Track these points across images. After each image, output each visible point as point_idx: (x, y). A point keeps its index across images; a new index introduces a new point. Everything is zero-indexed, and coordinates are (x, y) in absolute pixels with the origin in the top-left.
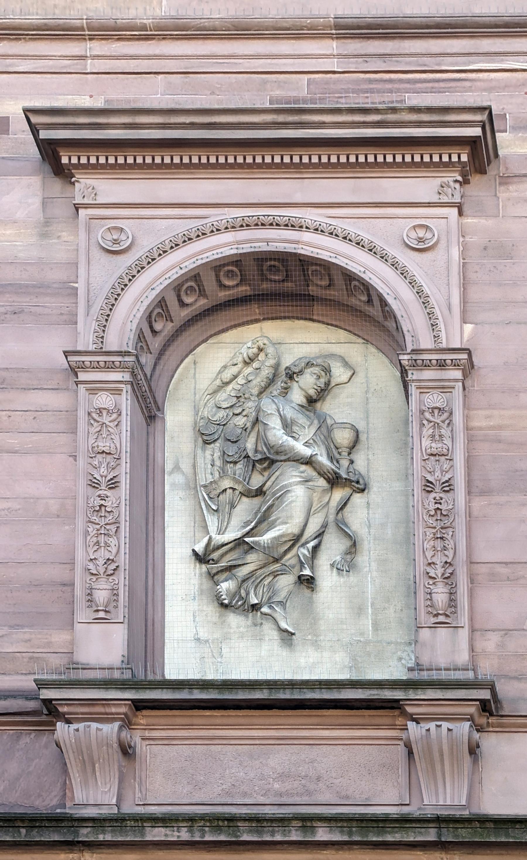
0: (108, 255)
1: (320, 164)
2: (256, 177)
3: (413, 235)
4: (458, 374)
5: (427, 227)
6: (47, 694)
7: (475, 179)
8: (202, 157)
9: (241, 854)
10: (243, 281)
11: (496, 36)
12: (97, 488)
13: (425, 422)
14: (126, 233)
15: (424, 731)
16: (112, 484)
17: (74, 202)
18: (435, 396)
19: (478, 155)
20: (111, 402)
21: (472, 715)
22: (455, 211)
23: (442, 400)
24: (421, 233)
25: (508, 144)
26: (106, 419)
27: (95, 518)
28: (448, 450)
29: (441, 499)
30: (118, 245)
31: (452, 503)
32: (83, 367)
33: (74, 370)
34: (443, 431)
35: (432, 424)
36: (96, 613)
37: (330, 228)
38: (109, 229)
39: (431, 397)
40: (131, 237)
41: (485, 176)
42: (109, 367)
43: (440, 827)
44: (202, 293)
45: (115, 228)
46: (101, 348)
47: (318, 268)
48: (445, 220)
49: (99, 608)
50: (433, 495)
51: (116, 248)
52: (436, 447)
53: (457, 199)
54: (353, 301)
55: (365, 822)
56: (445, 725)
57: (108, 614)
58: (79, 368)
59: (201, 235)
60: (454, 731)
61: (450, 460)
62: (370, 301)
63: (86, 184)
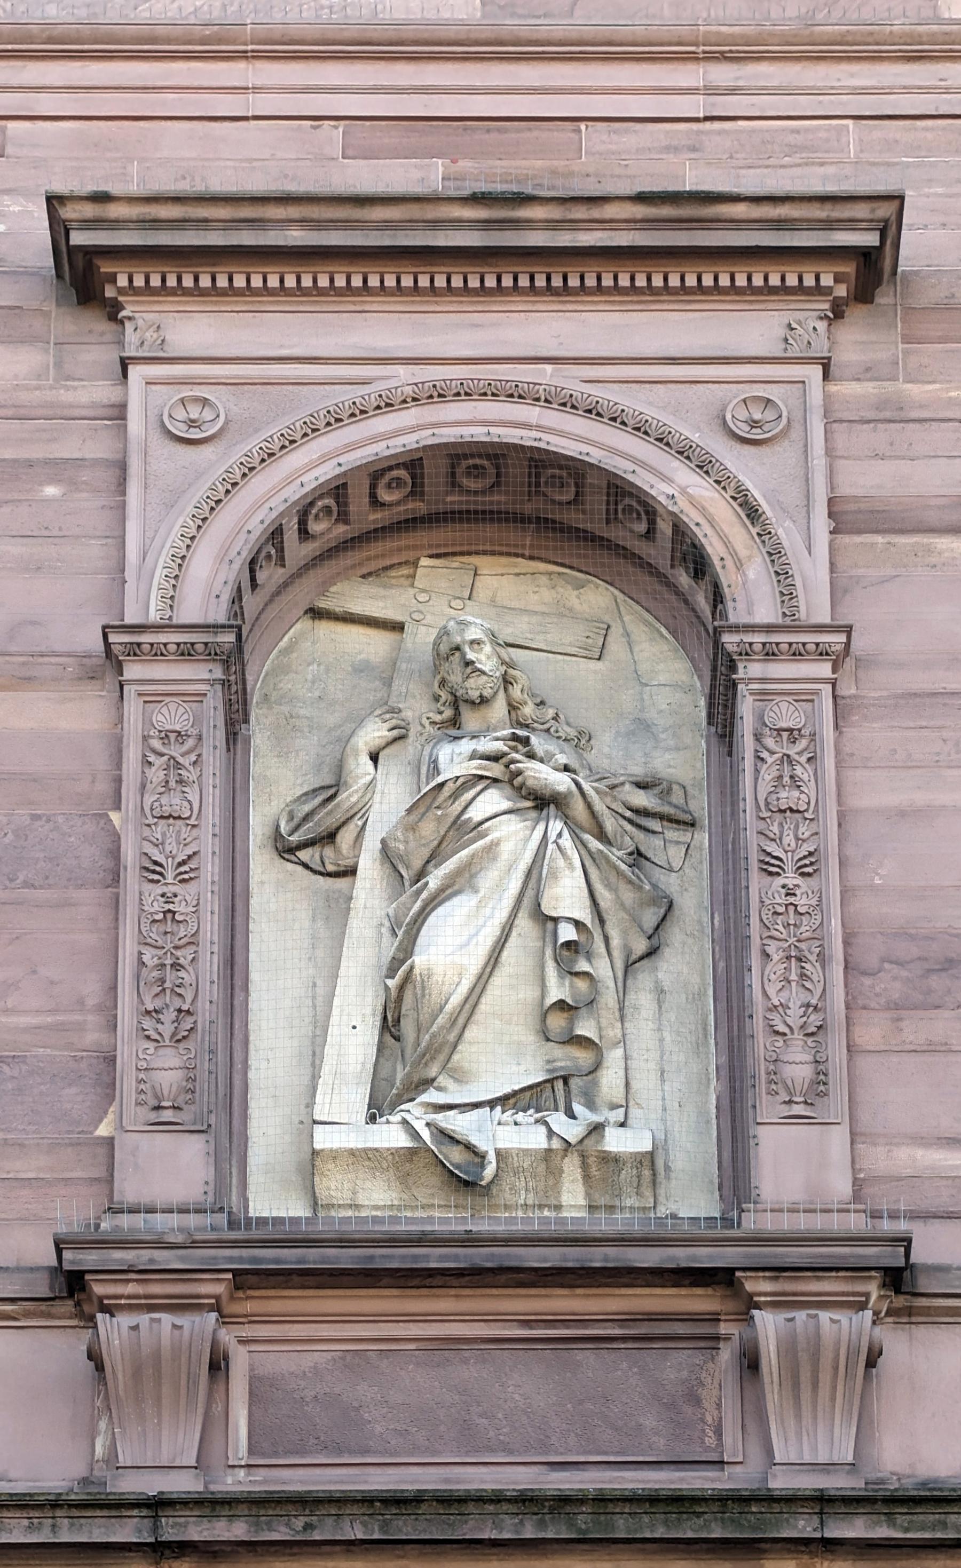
0: (738, 446)
1: (248, 290)
2: (223, 309)
3: (181, 414)
4: (824, 669)
5: (205, 402)
7: (856, 313)
8: (168, 276)
9: (478, 1560)
12: (778, 874)
13: (765, 755)
18: (173, 707)
19: (870, 272)
20: (185, 716)
21: (218, 1298)
22: (816, 372)
23: (185, 716)
24: (194, 412)
25: (916, 248)
28: (808, 803)
29: (176, 896)
30: (759, 431)
31: (195, 903)
33: (113, 660)
34: (799, 770)
35: (166, 758)
38: (744, 401)
39: (165, 710)
41: (869, 306)
43: (821, 1513)
44: (343, 517)
45: (197, 400)
46: (170, 618)
48: (800, 385)
51: (195, 434)
53: (820, 348)
54: (617, 534)
58: (741, 654)
59: (359, 413)
61: (194, 826)
62: (650, 534)
63: (147, 322)
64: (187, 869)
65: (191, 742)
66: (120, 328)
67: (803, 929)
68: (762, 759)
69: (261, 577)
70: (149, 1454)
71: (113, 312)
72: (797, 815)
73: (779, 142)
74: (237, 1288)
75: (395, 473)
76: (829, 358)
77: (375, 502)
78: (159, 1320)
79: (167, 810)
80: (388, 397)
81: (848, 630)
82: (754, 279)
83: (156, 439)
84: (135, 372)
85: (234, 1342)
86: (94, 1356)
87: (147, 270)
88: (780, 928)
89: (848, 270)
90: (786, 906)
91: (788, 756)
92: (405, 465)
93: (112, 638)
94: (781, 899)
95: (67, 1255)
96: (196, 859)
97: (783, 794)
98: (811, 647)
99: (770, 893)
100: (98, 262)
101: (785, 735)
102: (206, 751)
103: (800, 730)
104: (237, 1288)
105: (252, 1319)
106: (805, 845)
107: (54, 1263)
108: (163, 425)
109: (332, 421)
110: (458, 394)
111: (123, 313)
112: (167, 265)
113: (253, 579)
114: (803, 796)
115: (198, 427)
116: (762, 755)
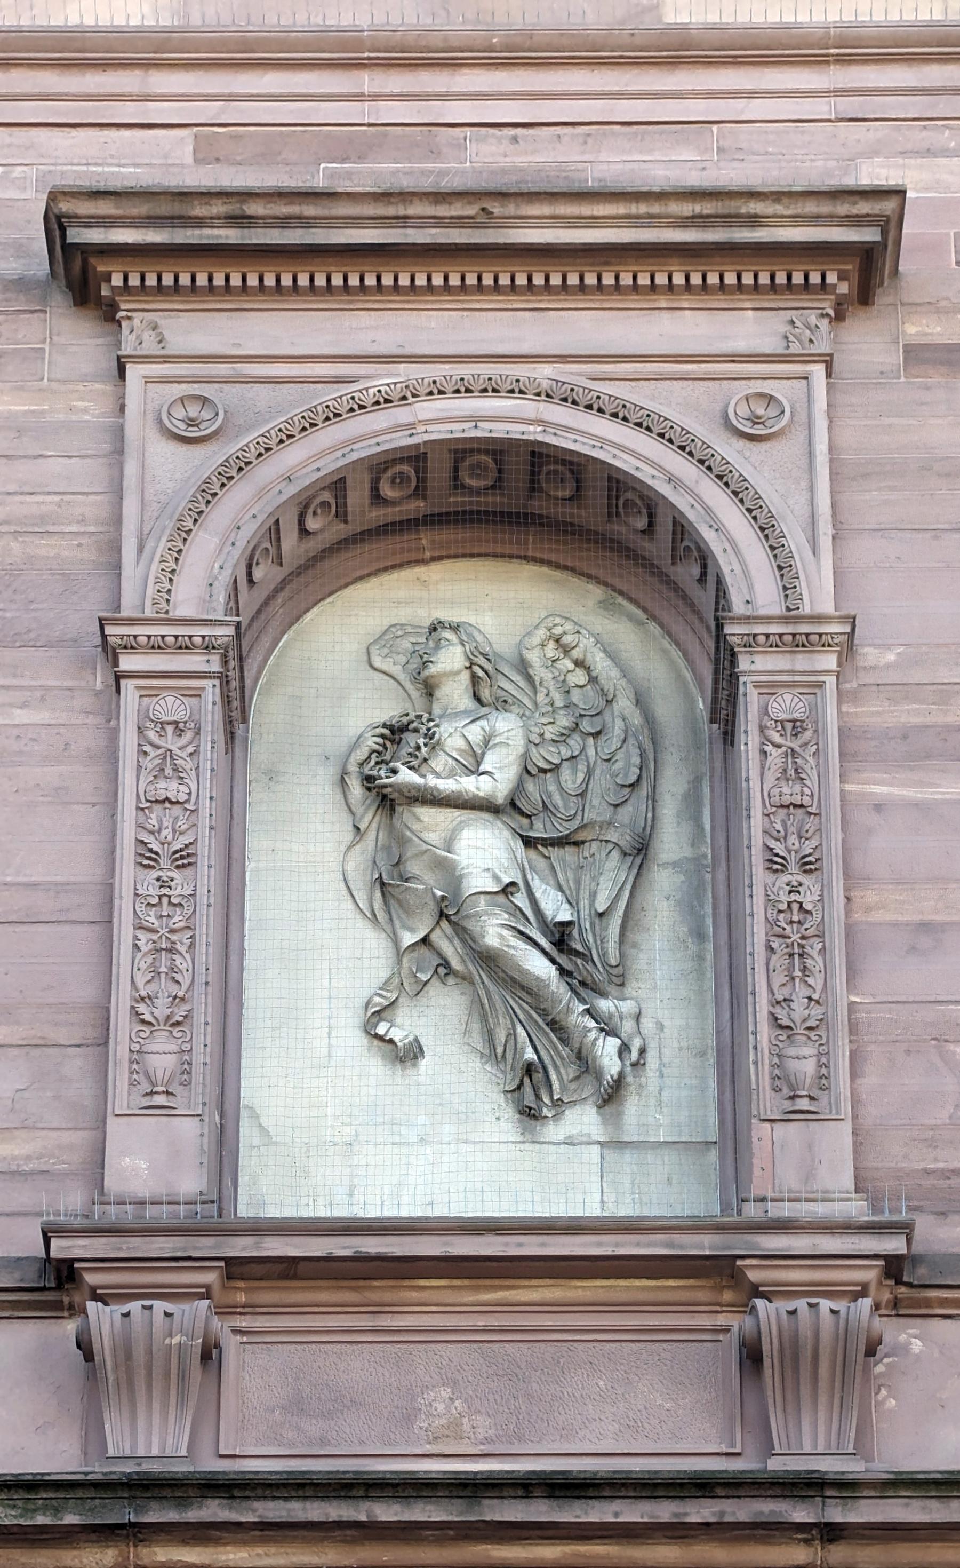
3: (179, 413)
5: (205, 401)
6: (60, 1248)
10: (420, 492)
11: (399, 65)
12: (154, 867)
14: (780, 403)
15: (117, 1317)
16: (182, 857)
17: (120, 353)
21: (208, 1287)
22: (818, 370)
24: (193, 410)
26: (171, 742)
27: (152, 919)
28: (189, 794)
29: (800, 885)
30: (761, 426)
32: (131, 647)
35: (784, 749)
36: (148, 1098)
37: (589, 397)
40: (221, 413)
42: (184, 646)
44: (342, 515)
45: (761, 395)
46: (167, 612)
47: (560, 468)
48: (804, 382)
49: (155, 1089)
50: (785, 878)
52: (790, 792)
53: (823, 347)
55: (470, 1488)
56: (160, 1306)
57: (171, 1097)
58: (125, 647)
60: (177, 1318)
64: (184, 859)
65: (189, 735)
66: (115, 326)
67: (176, 919)
68: (145, 753)
69: (258, 574)
70: (155, 1440)
71: (109, 314)
72: (178, 807)
73: (782, 143)
74: (230, 1277)
75: (398, 468)
76: (831, 355)
77: (377, 497)
78: (151, 1307)
79: (786, 800)
80: (386, 393)
81: (853, 621)
82: (450, 278)
83: (153, 434)
84: (134, 372)
85: (227, 1331)
86: (84, 1345)
87: (739, 268)
88: (152, 920)
89: (850, 267)
90: (160, 897)
91: (171, 751)
92: (409, 459)
93: (109, 630)
94: (154, 891)
95: (54, 1243)
96: (818, 850)
97: (162, 784)
98: (197, 640)
99: (145, 885)
100: (92, 261)
101: (170, 729)
102: (205, 746)
103: (185, 723)
104: (230, 1277)
105: (250, 1309)
106: (181, 838)
107: (43, 1254)
108: (160, 422)
109: (331, 415)
110: (512, 391)
111: (121, 314)
112: (690, 265)
113: (249, 574)
114: (182, 788)
115: (762, 423)
116: (145, 748)
